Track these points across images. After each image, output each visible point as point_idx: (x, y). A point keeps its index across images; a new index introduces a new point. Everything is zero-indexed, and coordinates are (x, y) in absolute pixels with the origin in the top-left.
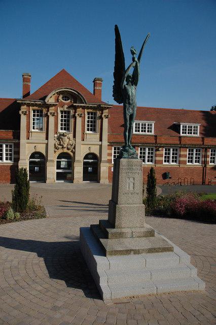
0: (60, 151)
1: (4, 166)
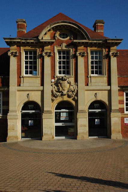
0: (59, 99)
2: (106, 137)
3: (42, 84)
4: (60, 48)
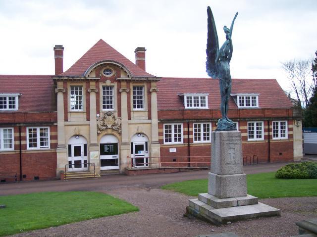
1: (38, 153)
3: (88, 119)
4: (105, 85)
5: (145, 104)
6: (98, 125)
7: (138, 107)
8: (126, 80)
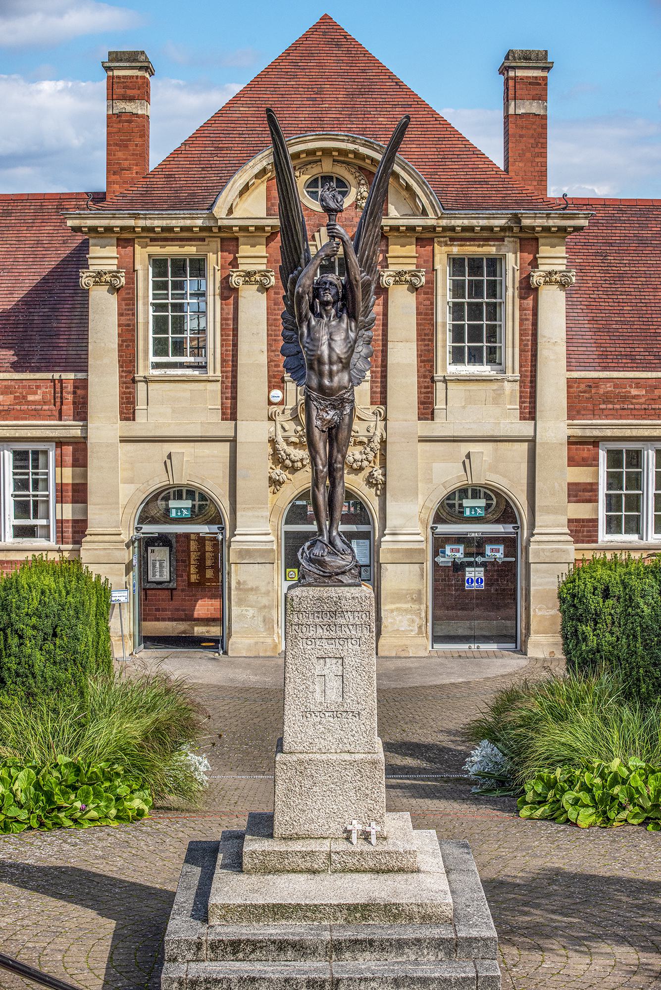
2: (513, 646)
3: (230, 413)
5: (511, 352)
6: (273, 442)
7: (475, 357)
8: (411, 229)
